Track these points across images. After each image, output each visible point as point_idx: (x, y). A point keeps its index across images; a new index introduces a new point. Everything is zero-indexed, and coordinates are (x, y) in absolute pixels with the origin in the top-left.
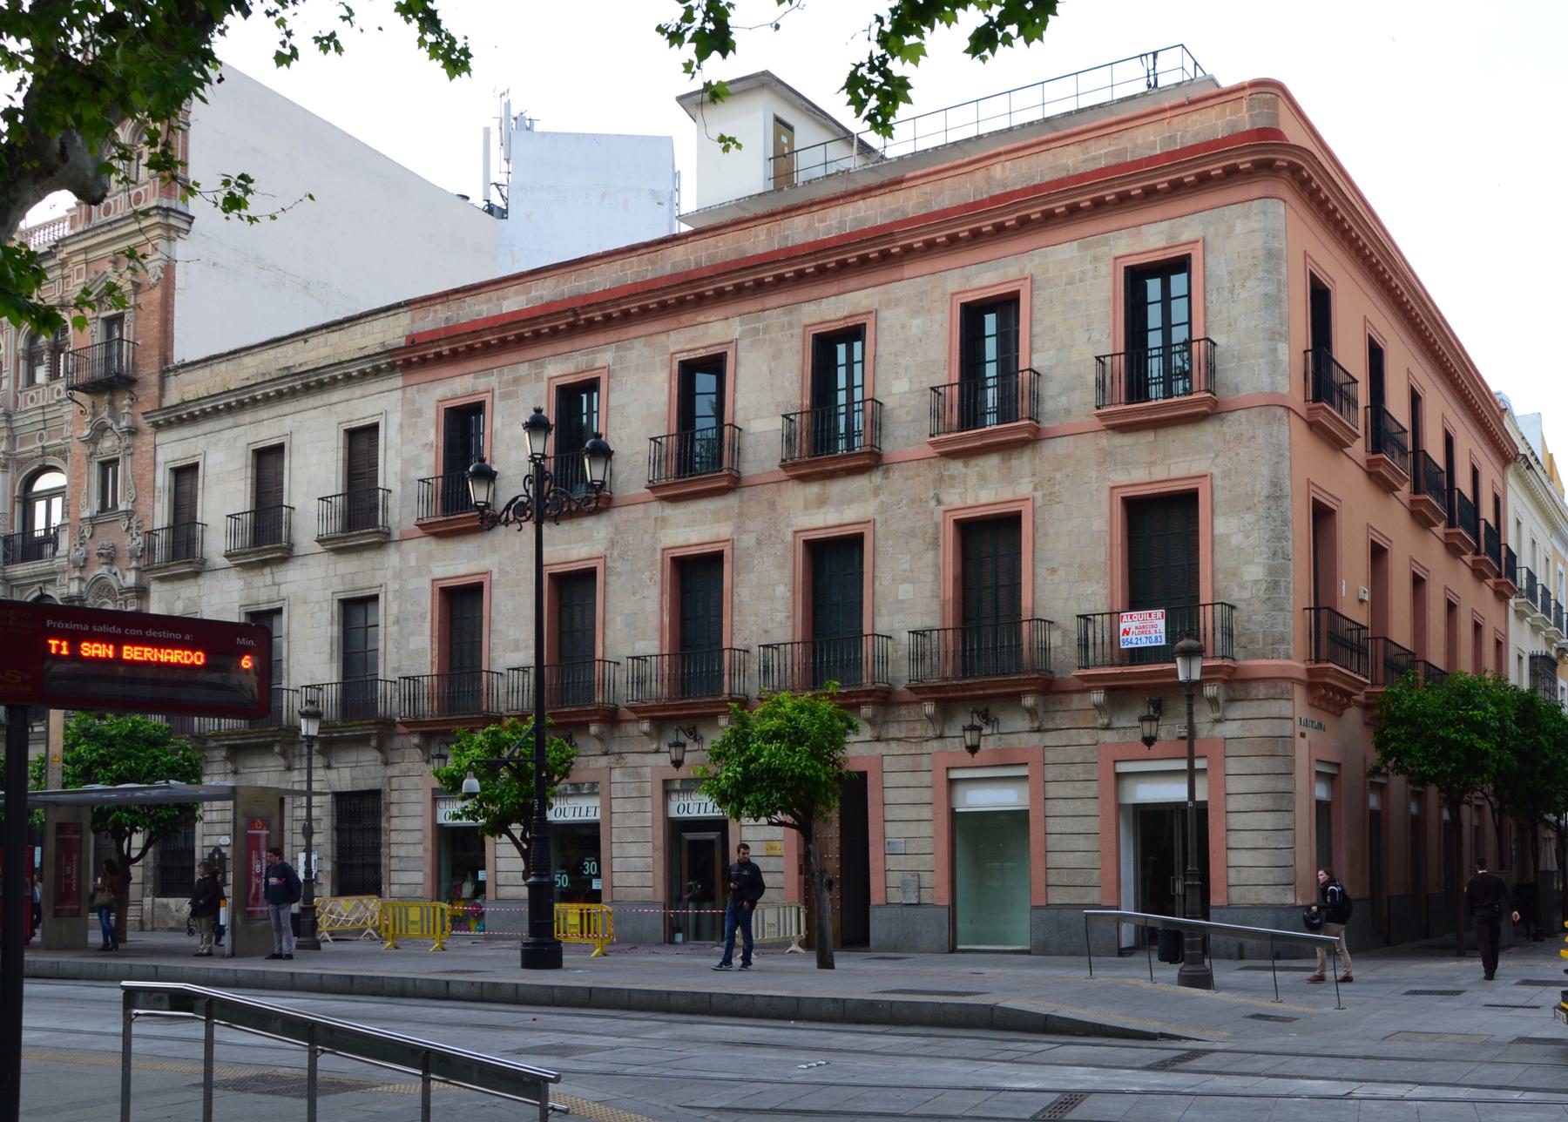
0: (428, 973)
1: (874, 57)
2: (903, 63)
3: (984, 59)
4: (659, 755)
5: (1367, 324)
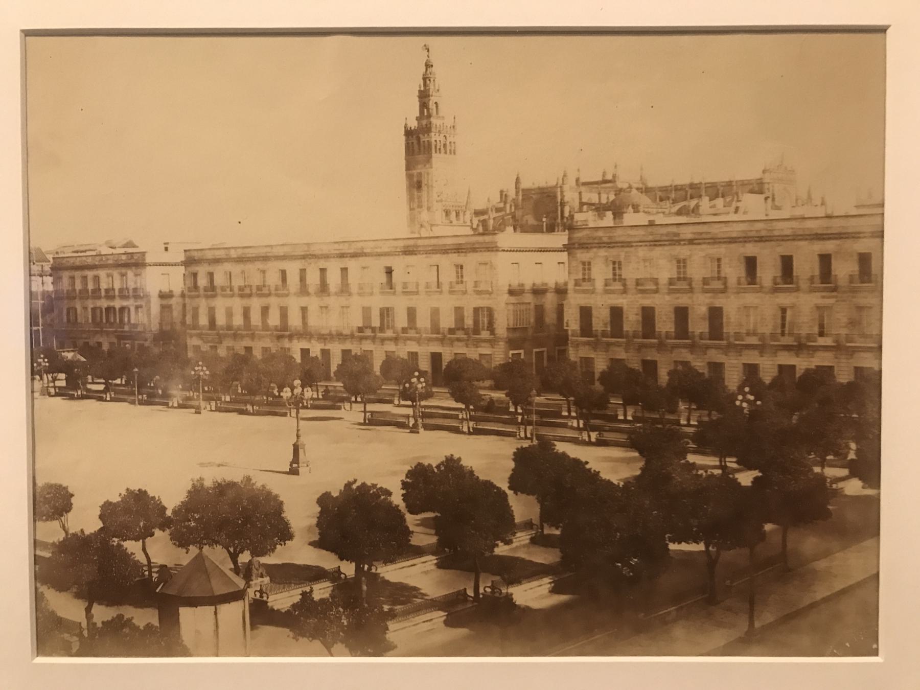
3: (471, 467)
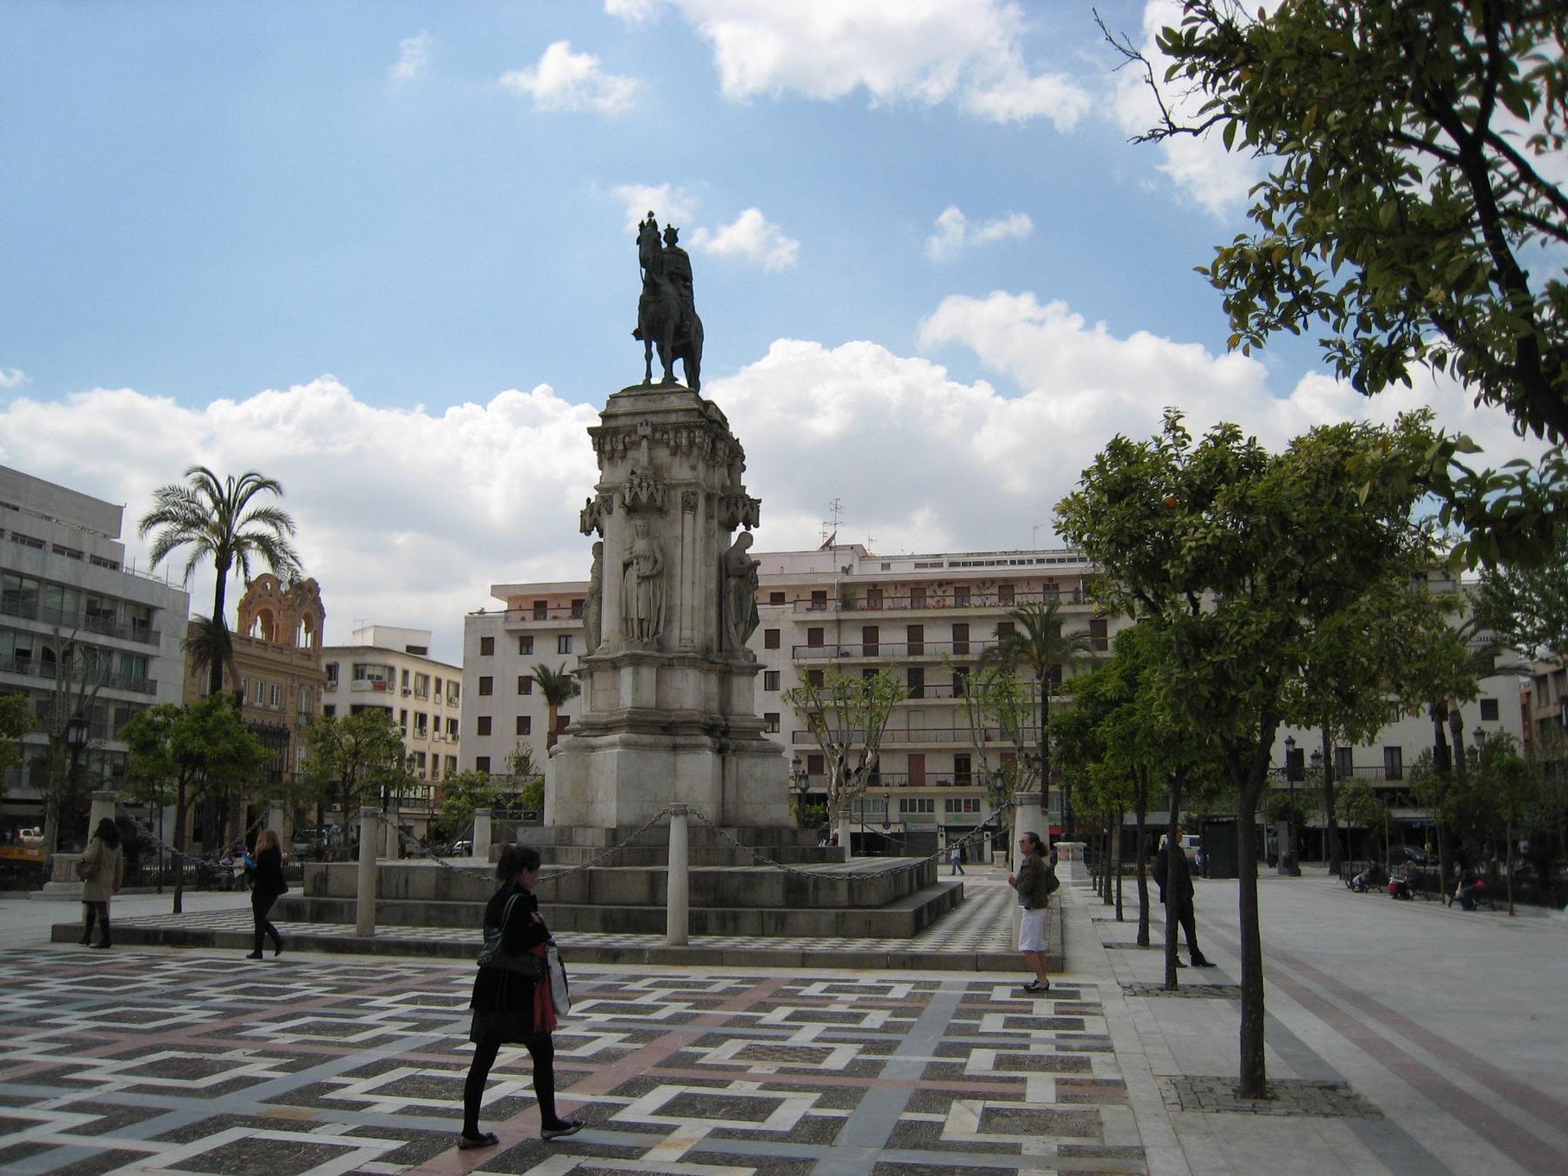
0: (746, 989)
1: (1002, 1030)
2: (1218, 248)
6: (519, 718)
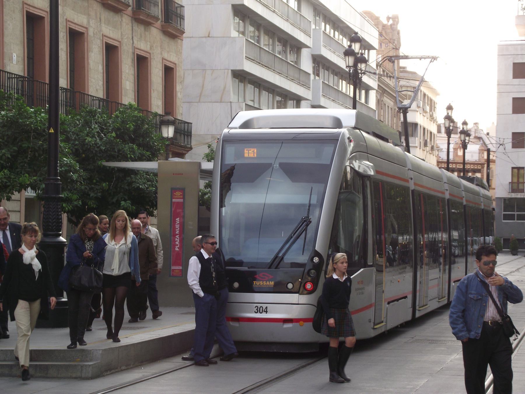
4: (208, 38)
5: (304, 232)
6: (514, 134)
